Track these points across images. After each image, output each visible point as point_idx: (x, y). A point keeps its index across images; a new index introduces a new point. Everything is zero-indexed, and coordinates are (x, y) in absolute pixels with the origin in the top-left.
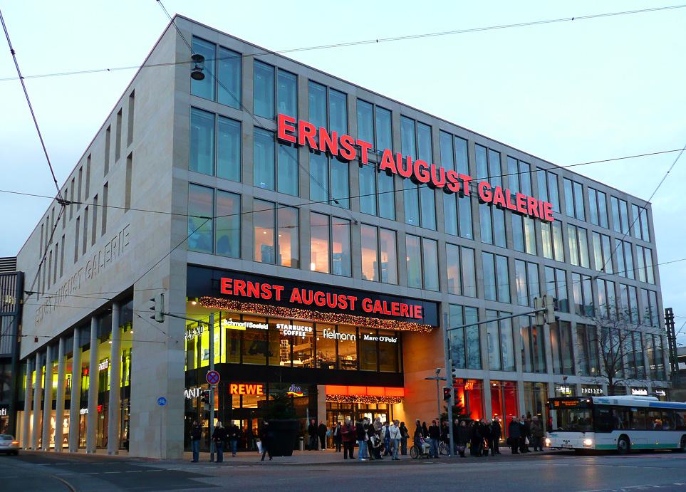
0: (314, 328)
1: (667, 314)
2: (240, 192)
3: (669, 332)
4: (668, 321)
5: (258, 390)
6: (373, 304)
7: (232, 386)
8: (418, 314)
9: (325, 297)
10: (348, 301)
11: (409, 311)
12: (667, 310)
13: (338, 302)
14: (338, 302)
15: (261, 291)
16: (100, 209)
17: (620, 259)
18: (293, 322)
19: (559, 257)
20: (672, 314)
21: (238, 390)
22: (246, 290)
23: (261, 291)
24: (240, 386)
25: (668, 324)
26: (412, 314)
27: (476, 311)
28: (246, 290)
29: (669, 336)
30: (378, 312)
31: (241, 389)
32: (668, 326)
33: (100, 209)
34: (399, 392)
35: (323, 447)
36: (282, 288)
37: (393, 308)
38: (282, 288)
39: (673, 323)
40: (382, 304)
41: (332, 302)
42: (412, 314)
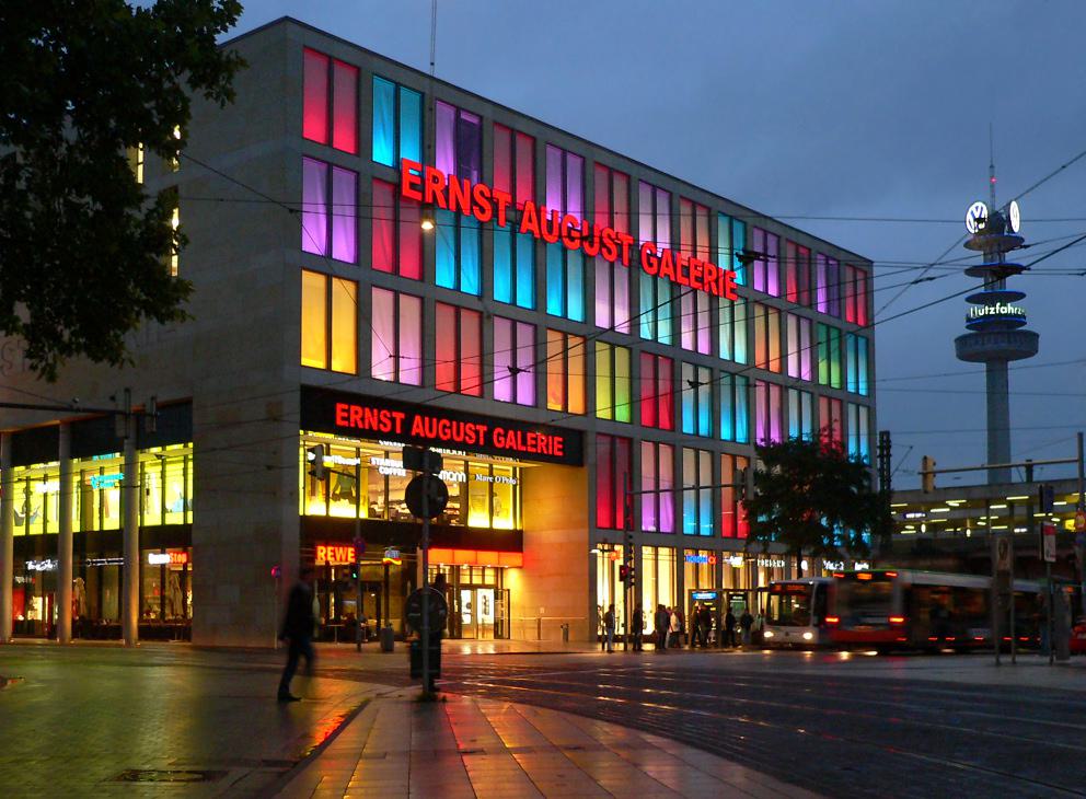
0: (421, 462)
1: (882, 441)
2: (422, 295)
3: (881, 470)
4: (882, 451)
5: (350, 555)
6: (506, 435)
7: (320, 548)
8: (559, 450)
9: (450, 428)
10: (477, 432)
11: (547, 446)
12: (882, 434)
13: (466, 434)
14: (466, 434)
15: (380, 422)
16: (861, 299)
17: (444, 350)
18: (390, 455)
19: (774, 366)
20: (889, 441)
21: (326, 555)
22: (363, 419)
23: (380, 422)
24: (330, 548)
25: (881, 456)
26: (550, 450)
27: (626, 445)
28: (363, 419)
29: (882, 476)
30: (511, 447)
31: (330, 554)
32: (882, 461)
33: (861, 299)
34: (516, 558)
35: (302, 552)
36: (402, 416)
37: (530, 442)
38: (402, 416)
39: (889, 456)
40: (516, 435)
41: (458, 434)
42: (550, 450)
